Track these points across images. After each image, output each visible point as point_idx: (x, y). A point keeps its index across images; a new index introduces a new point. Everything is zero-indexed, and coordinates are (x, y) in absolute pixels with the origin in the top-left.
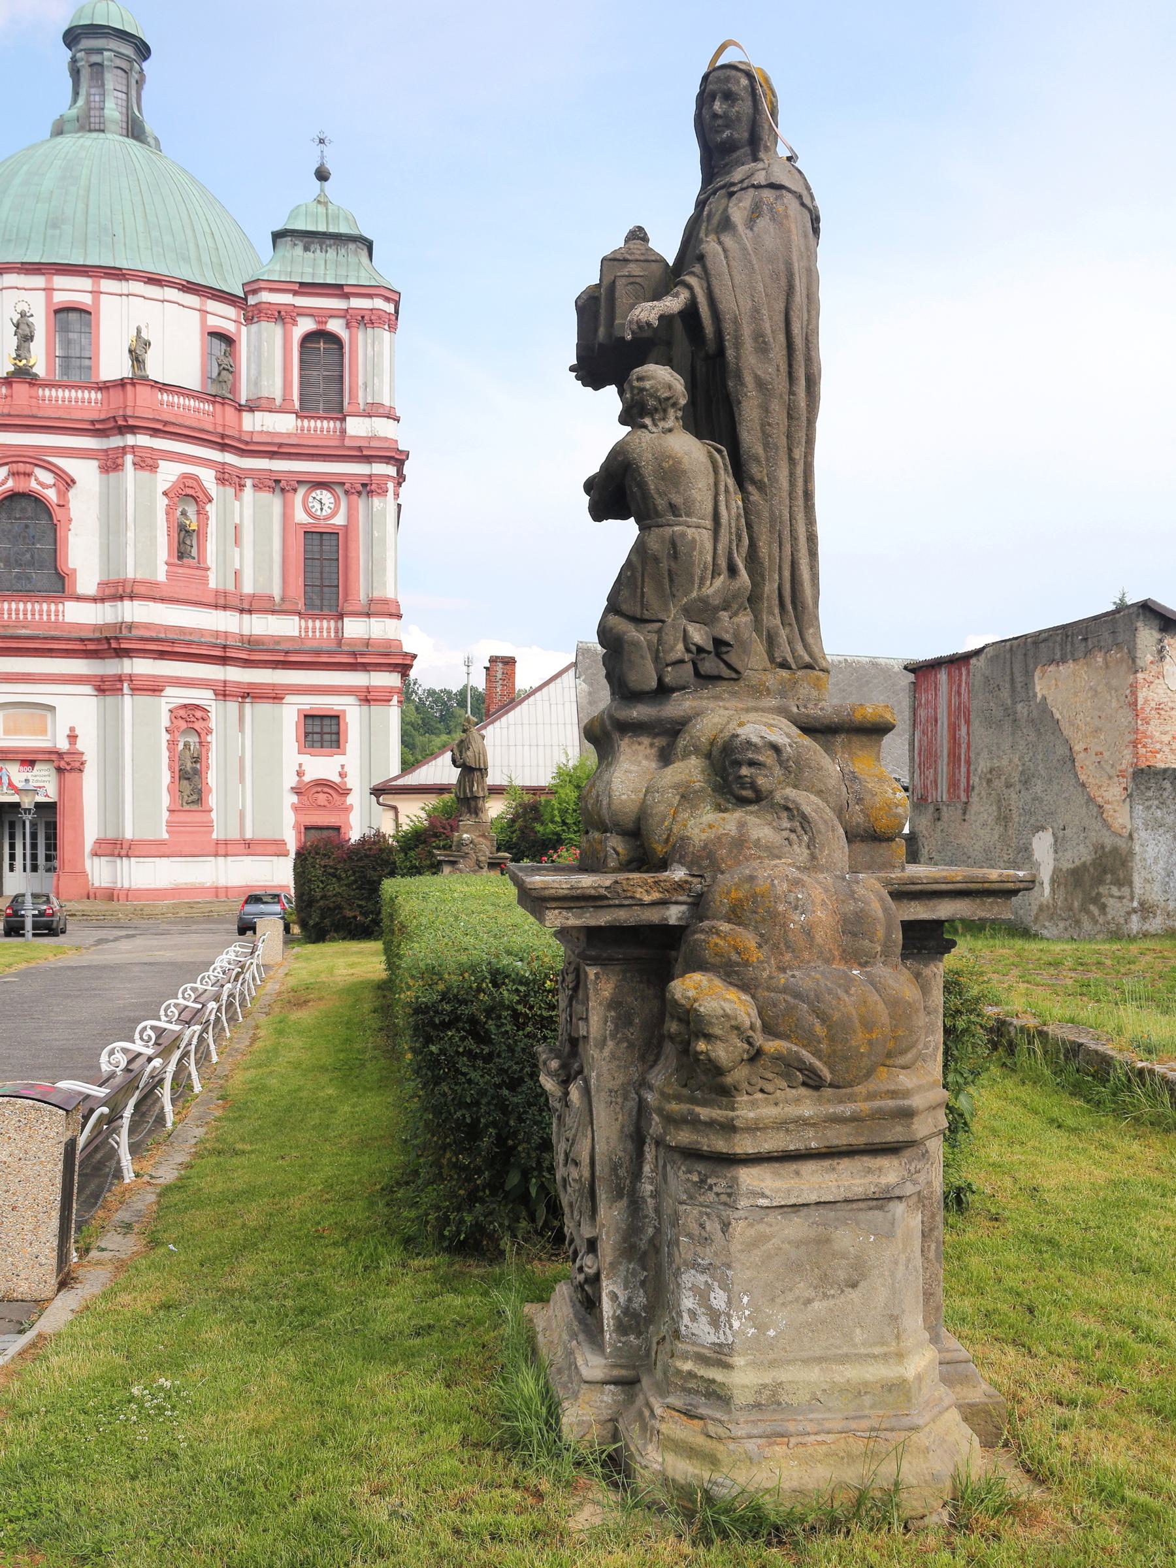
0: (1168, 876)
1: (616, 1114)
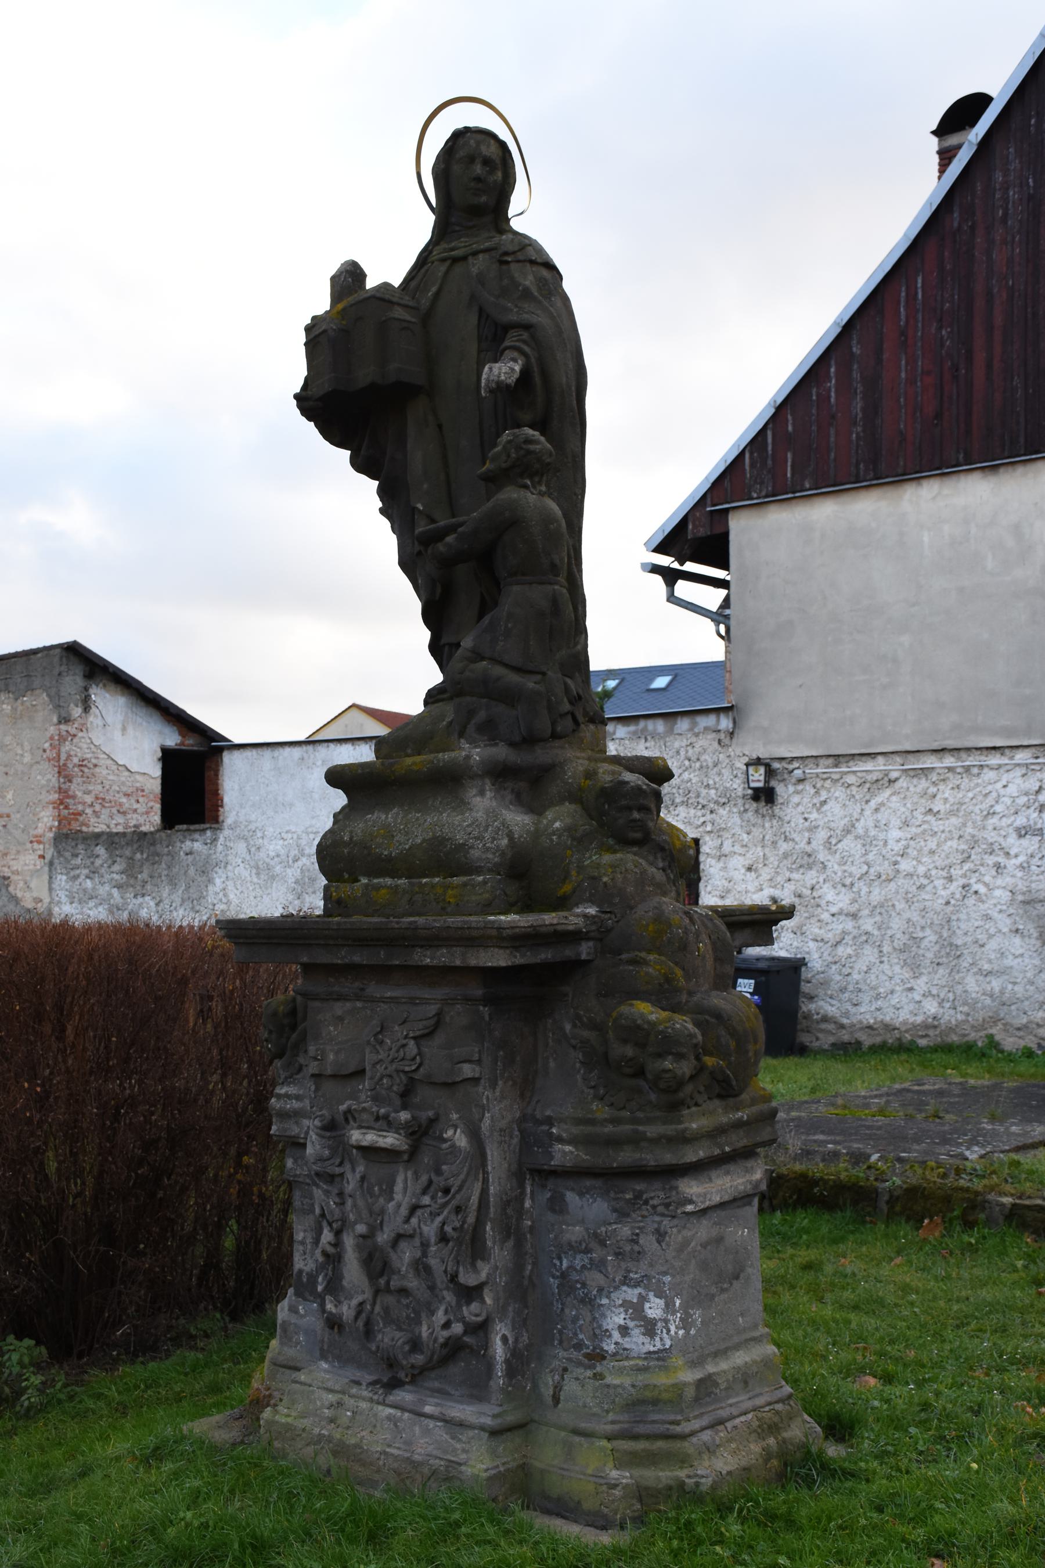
1: (505, 1152)
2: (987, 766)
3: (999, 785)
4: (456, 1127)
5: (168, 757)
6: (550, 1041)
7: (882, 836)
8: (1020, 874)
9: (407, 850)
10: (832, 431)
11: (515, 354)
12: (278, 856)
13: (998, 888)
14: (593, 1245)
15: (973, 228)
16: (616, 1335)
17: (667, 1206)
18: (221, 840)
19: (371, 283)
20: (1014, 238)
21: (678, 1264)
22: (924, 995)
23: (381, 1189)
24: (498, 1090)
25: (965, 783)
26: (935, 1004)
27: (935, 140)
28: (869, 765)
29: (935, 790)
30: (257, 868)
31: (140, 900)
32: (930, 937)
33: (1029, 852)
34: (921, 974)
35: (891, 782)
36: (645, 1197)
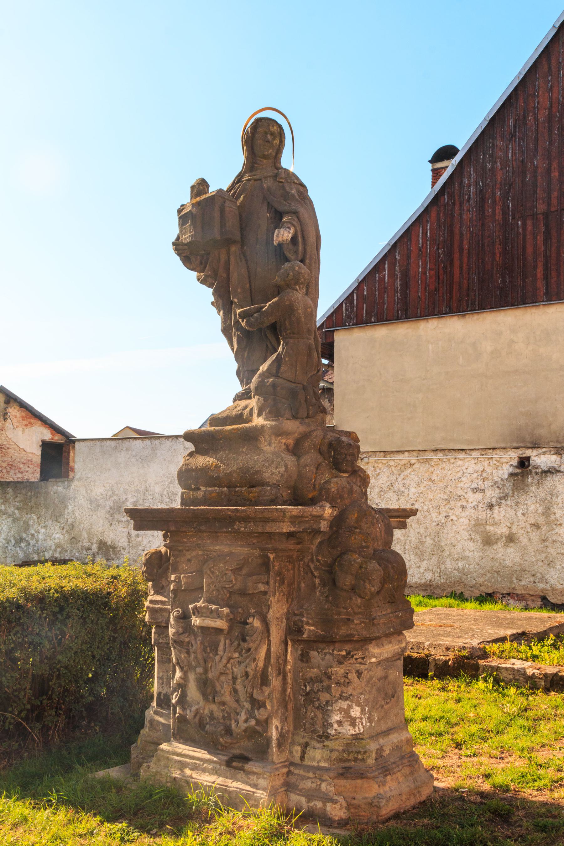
0: (8, 543)
2: (459, 458)
3: (464, 468)
4: (254, 617)
5: (45, 445)
6: (302, 572)
7: (406, 491)
8: (473, 511)
9: (228, 474)
10: (386, 296)
11: (289, 225)
12: (102, 495)
13: (463, 517)
14: (324, 678)
15: (454, 203)
16: (336, 726)
17: (363, 658)
18: (73, 487)
19: (213, 189)
20: (473, 209)
21: (367, 689)
22: (425, 570)
23: (211, 649)
24: (276, 597)
25: (447, 466)
26: (431, 575)
27: (430, 165)
28: (400, 457)
29: (433, 469)
30: (91, 501)
31: (29, 516)
32: (429, 541)
33: (478, 500)
34: (424, 560)
35: (412, 465)
36: (352, 653)
